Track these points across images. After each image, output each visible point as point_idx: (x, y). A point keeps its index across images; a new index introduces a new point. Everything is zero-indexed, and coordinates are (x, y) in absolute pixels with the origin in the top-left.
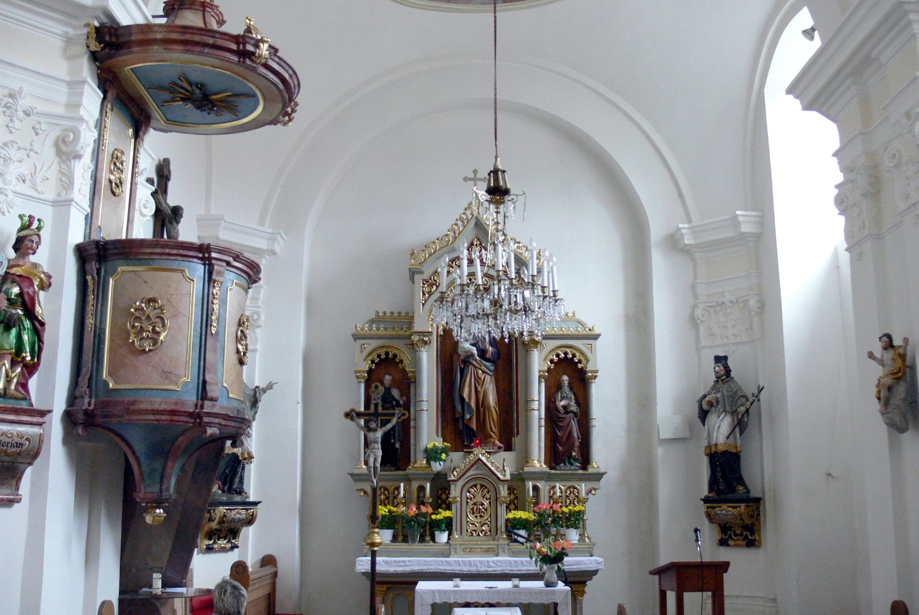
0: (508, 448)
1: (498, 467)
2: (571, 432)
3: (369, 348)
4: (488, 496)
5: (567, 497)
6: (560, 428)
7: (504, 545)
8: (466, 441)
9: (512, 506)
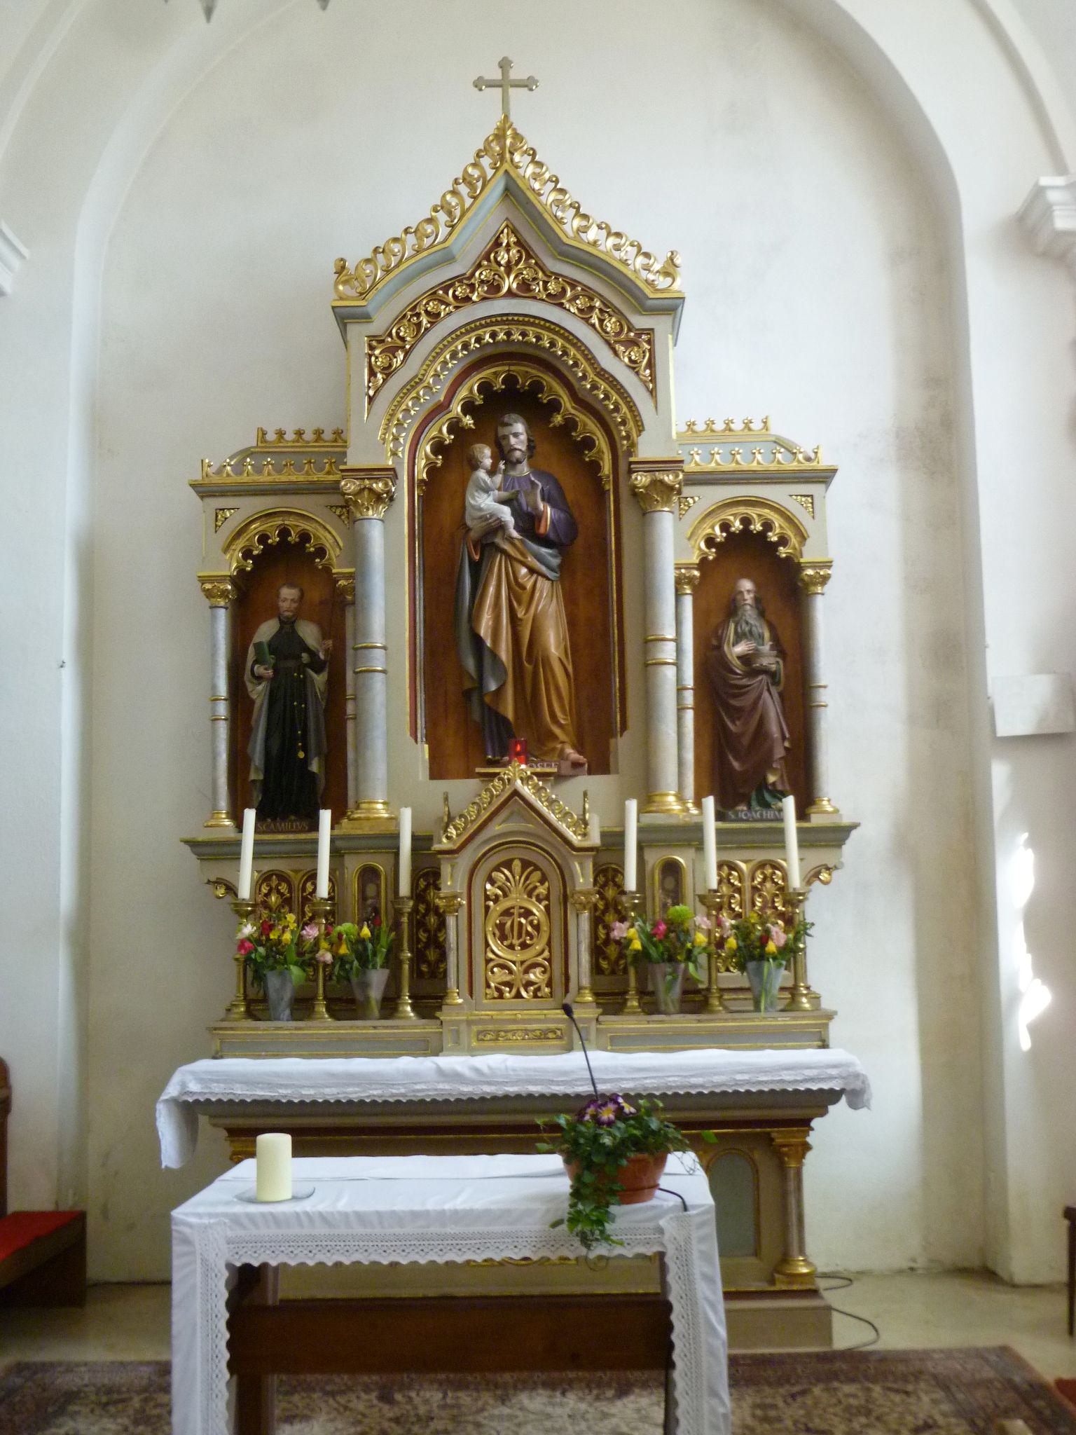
0: (600, 764)
1: (567, 814)
3: (234, 520)
4: (542, 890)
5: (755, 889)
6: (736, 713)
7: (588, 1020)
8: (490, 751)
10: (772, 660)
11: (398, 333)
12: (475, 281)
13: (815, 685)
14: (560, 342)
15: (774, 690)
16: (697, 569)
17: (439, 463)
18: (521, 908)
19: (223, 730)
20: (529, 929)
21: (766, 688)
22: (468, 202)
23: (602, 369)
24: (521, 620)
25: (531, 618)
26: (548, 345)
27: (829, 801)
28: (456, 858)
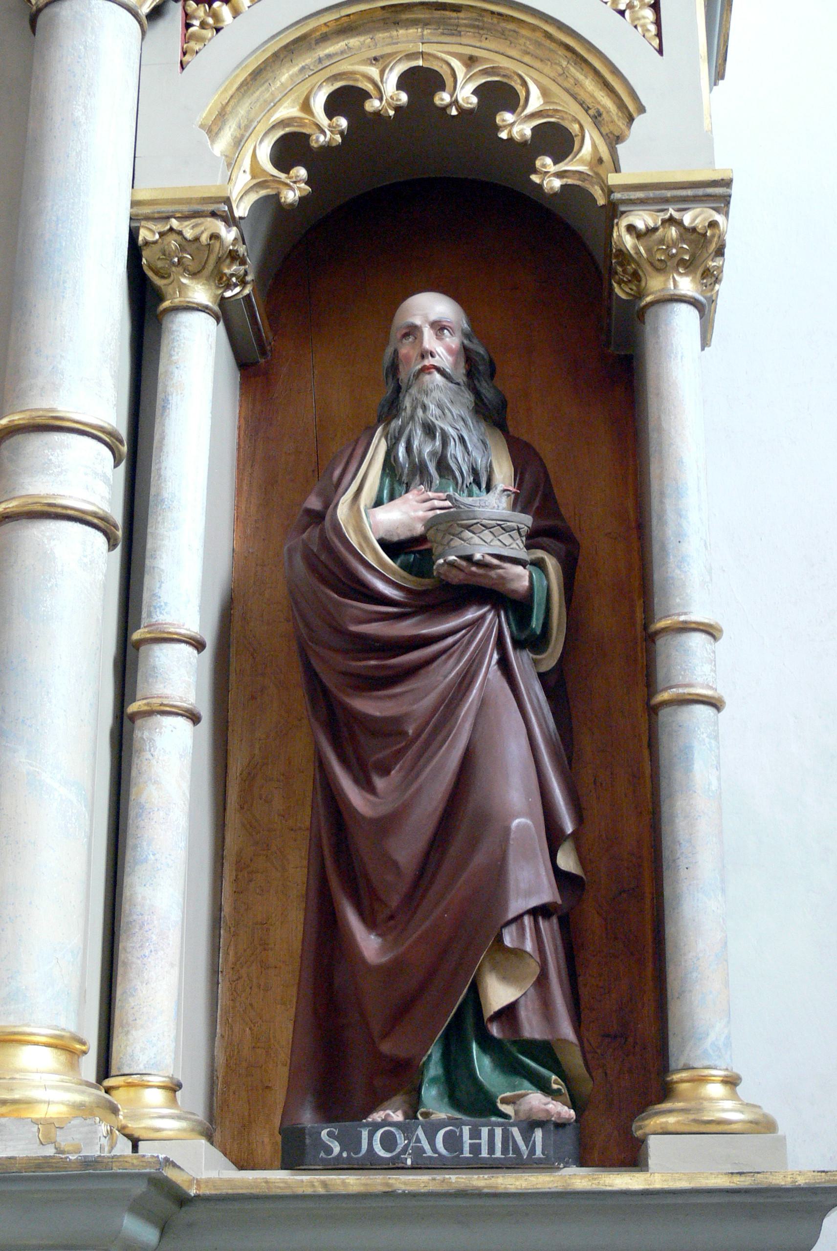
10: (516, 547)
15: (519, 660)
27: (732, 1082)
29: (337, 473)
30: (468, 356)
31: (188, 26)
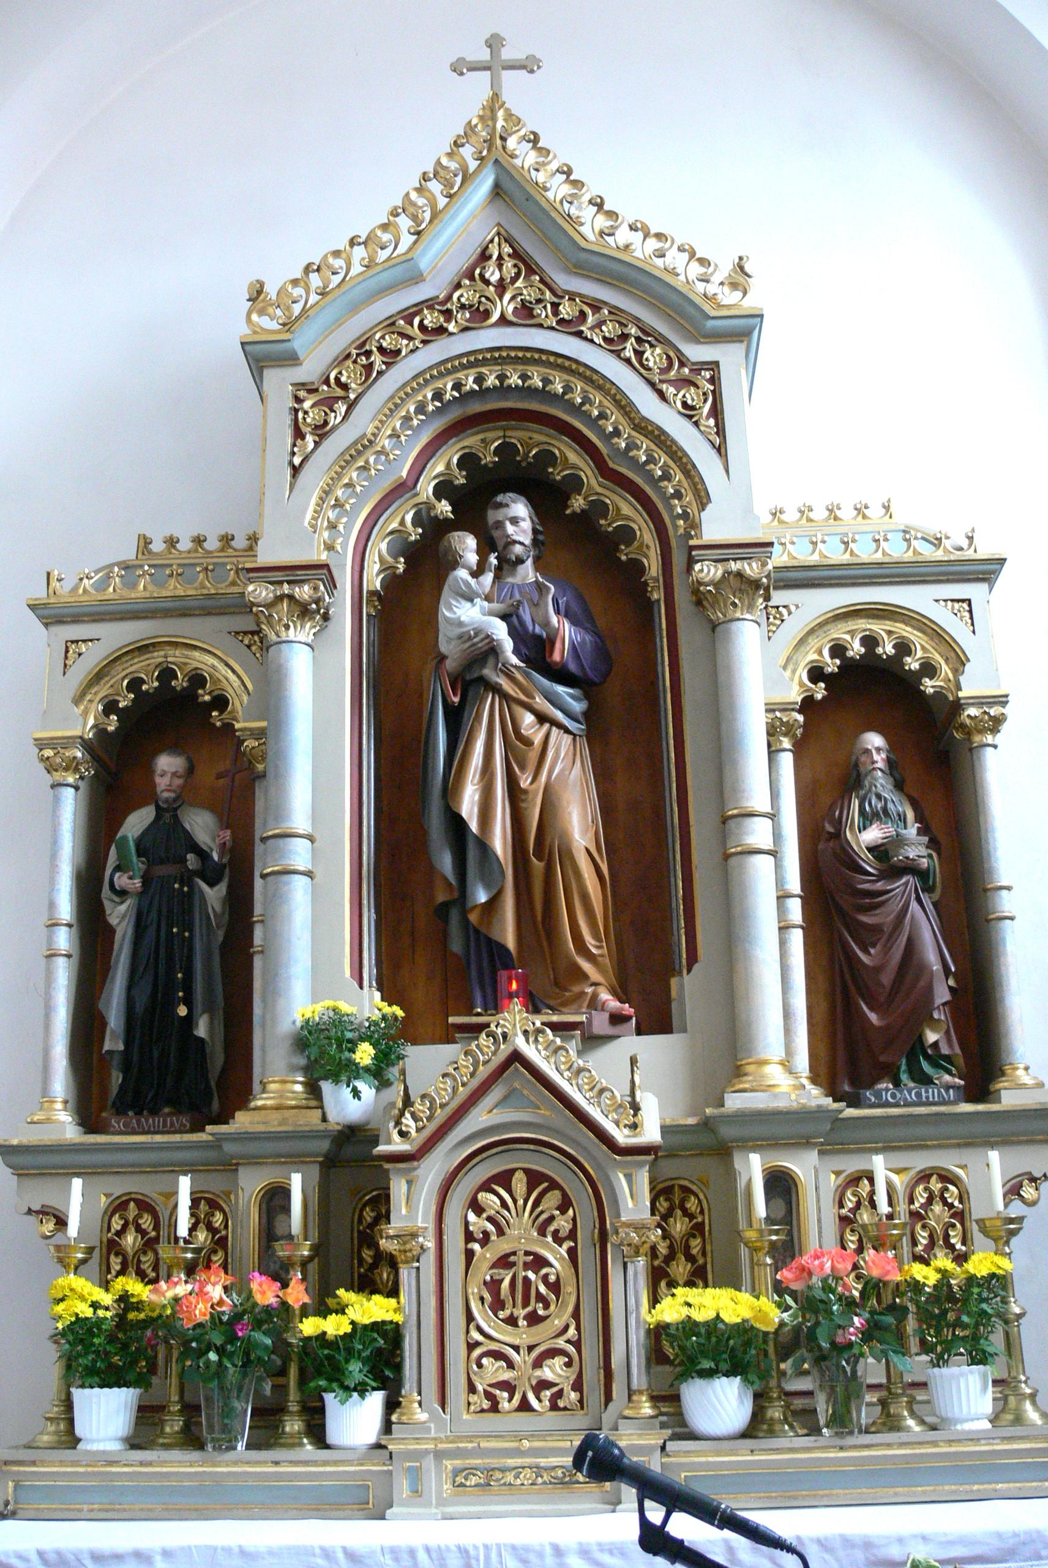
2: (911, 948)
3: (92, 657)
4: (563, 1224)
5: (915, 1216)
6: (868, 936)
9: (681, 1269)
10: (923, 851)
11: (337, 380)
12: (453, 306)
13: (989, 886)
14: (579, 386)
16: (800, 712)
17: (401, 568)
18: (527, 1253)
19: (63, 976)
20: (543, 1289)
21: (913, 896)
22: (442, 202)
23: (644, 418)
24: (525, 792)
25: (542, 786)
26: (561, 390)
27: (1027, 1069)
28: (415, 1169)
29: (837, 813)
30: (889, 761)
31: (768, 619)
